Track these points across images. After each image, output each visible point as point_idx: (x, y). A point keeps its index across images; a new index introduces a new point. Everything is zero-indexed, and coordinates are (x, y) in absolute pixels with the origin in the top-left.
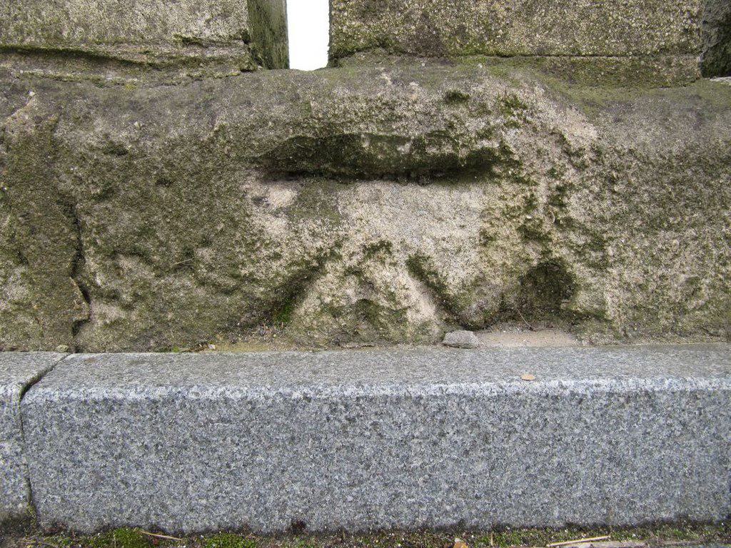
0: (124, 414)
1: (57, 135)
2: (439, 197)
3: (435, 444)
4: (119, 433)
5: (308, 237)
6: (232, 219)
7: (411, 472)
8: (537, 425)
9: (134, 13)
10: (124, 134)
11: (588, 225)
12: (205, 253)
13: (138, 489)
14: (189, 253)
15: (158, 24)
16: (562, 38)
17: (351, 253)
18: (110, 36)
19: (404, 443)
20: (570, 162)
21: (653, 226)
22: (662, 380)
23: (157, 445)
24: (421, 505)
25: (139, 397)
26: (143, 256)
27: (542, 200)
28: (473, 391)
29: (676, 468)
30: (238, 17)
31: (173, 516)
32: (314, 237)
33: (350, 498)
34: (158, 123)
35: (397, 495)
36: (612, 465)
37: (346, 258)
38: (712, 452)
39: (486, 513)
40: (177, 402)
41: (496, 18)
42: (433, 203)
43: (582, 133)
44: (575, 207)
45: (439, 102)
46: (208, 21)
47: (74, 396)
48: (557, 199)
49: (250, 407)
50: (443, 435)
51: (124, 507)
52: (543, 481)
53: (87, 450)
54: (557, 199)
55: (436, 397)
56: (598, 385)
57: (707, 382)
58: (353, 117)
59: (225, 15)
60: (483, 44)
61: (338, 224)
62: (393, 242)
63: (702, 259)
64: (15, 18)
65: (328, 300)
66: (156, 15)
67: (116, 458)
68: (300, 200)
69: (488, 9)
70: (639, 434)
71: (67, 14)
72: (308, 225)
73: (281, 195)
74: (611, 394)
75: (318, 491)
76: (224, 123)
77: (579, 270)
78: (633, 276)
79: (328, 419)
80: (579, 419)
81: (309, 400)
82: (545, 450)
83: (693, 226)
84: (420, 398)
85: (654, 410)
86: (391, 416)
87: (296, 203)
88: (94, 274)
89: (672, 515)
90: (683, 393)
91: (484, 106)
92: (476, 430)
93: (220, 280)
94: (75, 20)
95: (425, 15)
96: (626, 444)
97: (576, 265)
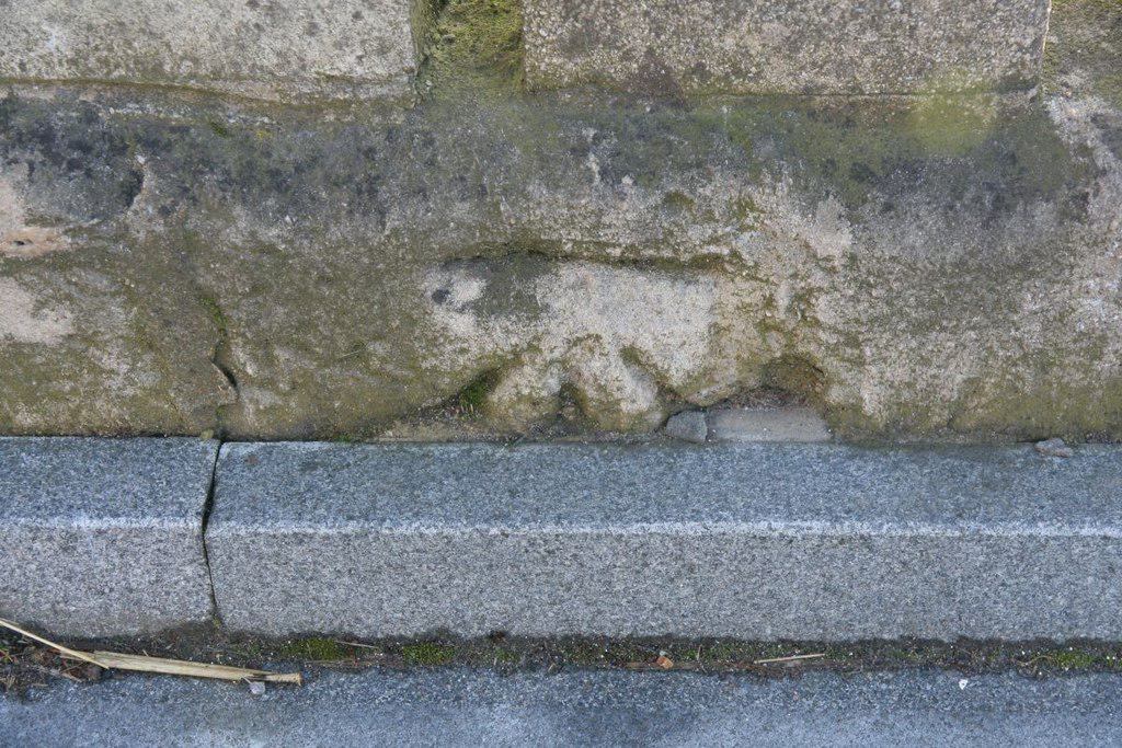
0: (317, 546)
1: (189, 226)
2: (662, 290)
3: (638, 572)
4: (310, 560)
5: (500, 335)
6: (410, 316)
7: (615, 595)
8: (745, 559)
9: (259, 47)
10: (274, 232)
11: (840, 327)
12: (379, 349)
13: (330, 605)
14: (359, 346)
15: (293, 59)
16: (838, 76)
17: (553, 347)
18: (228, 70)
19: (605, 571)
20: (817, 265)
21: (920, 328)
22: (881, 524)
23: (350, 571)
24: (625, 621)
25: (330, 532)
26: (305, 348)
27: (783, 300)
28: (677, 532)
29: (897, 599)
30: (400, 53)
31: (368, 627)
32: (503, 336)
33: (551, 614)
34: (313, 216)
35: (599, 612)
36: (826, 594)
37: (546, 353)
38: (937, 586)
39: (693, 629)
40: (370, 536)
41: (747, 55)
42: (651, 295)
43: (836, 242)
44: (823, 308)
45: (656, 208)
46: (360, 58)
47: (262, 530)
48: (803, 298)
49: (446, 540)
50: (646, 565)
51: (316, 620)
52: (754, 605)
53: (276, 573)
54: (803, 298)
55: (637, 535)
56: (809, 528)
57: (930, 529)
58: (552, 223)
59: (383, 51)
60: (729, 84)
61: (536, 318)
62: (603, 335)
63: (986, 360)
64: (97, 48)
65: (526, 392)
66: (289, 49)
67: (307, 580)
68: (489, 291)
69: (737, 45)
70: (855, 569)
71: (168, 45)
72: (498, 325)
73: (469, 289)
74: (822, 537)
75: (517, 609)
76: (397, 223)
77: (831, 364)
78: (899, 373)
79: (527, 551)
80: (790, 556)
81: (507, 536)
82: (753, 580)
83: (973, 328)
84: (622, 536)
85: (871, 550)
86: (592, 549)
87: (485, 296)
88: (244, 365)
89: (896, 637)
90: (902, 538)
91: (710, 212)
92: (681, 562)
93: (397, 372)
94: (180, 53)
95: (650, 51)
96: (841, 578)
97: (828, 360)
